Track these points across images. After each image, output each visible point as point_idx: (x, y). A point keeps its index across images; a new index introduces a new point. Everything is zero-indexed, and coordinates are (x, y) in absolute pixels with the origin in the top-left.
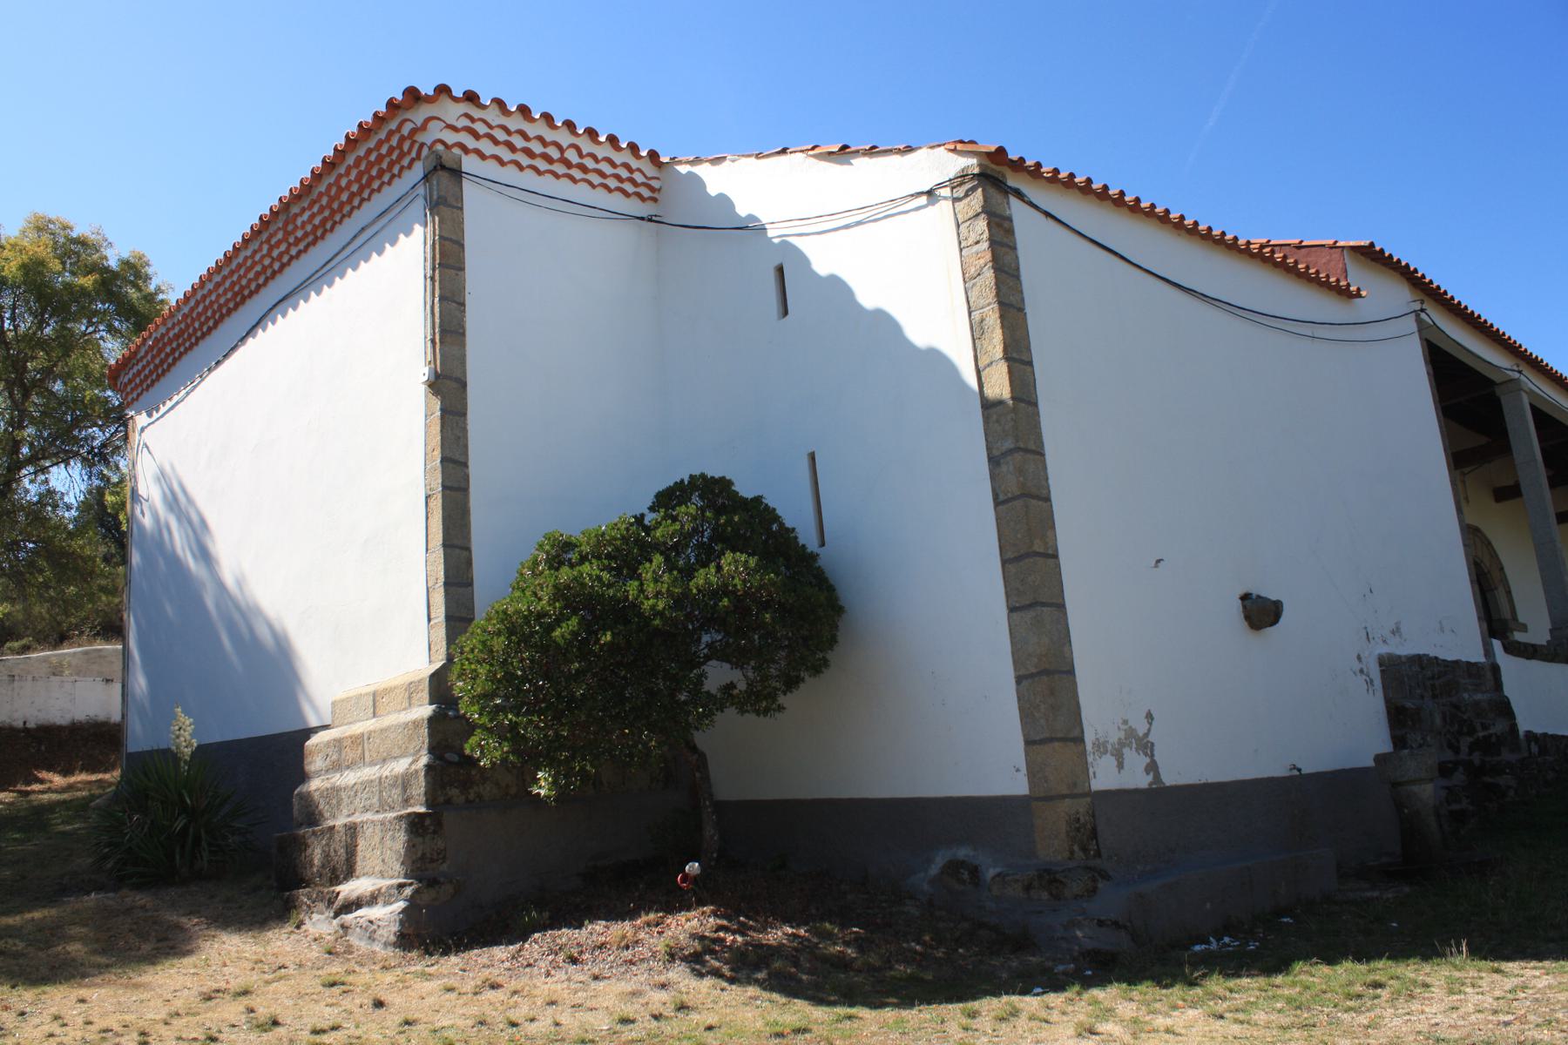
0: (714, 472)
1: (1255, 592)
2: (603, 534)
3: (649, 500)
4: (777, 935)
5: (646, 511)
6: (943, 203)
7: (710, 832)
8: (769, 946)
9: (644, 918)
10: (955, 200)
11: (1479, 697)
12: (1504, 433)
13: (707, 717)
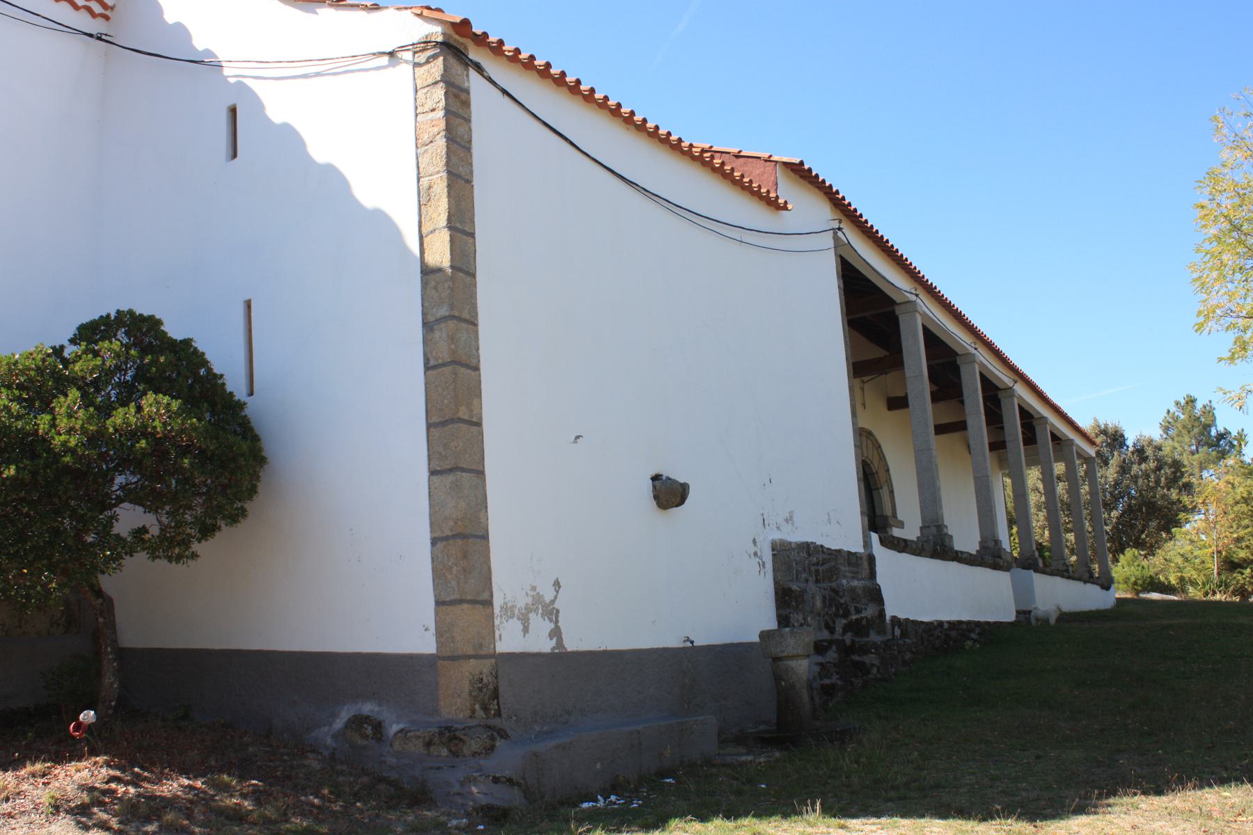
0: (143, 309)
1: (666, 473)
2: (16, 362)
3: (71, 331)
4: (173, 787)
5: (66, 343)
6: (404, 66)
7: (110, 681)
8: (163, 798)
9: (29, 768)
10: (416, 65)
11: (855, 583)
12: (899, 350)
13: (114, 560)
